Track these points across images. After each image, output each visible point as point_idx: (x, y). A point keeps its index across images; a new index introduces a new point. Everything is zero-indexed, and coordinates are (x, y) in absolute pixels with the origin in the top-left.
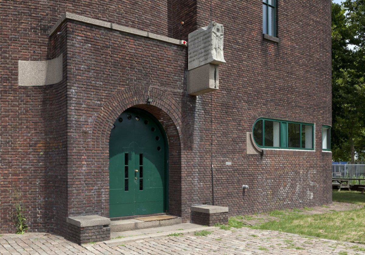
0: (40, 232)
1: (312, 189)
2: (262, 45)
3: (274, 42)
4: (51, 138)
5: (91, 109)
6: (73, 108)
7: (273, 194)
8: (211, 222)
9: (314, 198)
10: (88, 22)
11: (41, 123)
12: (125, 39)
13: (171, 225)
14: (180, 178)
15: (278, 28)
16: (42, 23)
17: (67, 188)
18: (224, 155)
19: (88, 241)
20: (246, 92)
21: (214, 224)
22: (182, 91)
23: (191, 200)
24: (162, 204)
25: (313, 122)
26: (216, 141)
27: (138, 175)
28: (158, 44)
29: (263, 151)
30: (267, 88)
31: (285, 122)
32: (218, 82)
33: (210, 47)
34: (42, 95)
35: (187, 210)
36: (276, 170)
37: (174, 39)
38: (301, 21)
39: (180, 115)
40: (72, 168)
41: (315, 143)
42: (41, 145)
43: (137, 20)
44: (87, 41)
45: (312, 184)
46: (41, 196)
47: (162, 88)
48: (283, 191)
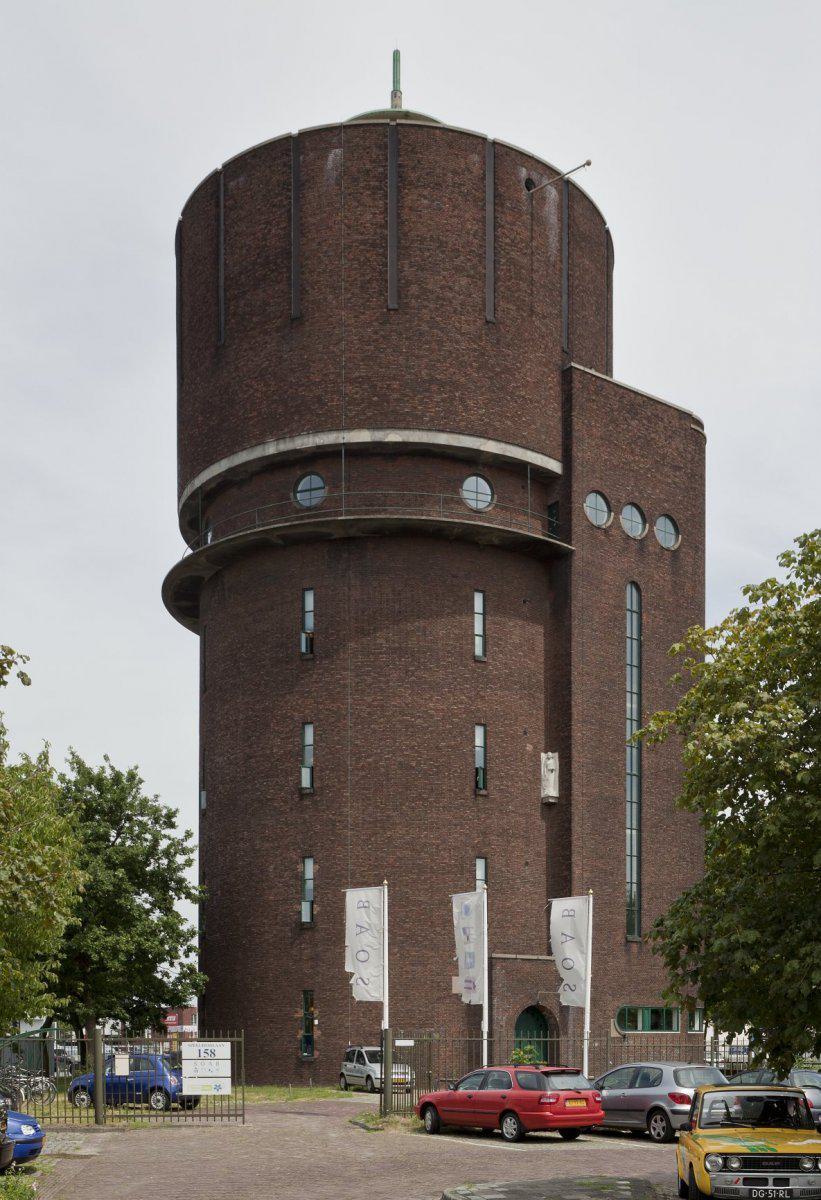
31: (647, 1008)
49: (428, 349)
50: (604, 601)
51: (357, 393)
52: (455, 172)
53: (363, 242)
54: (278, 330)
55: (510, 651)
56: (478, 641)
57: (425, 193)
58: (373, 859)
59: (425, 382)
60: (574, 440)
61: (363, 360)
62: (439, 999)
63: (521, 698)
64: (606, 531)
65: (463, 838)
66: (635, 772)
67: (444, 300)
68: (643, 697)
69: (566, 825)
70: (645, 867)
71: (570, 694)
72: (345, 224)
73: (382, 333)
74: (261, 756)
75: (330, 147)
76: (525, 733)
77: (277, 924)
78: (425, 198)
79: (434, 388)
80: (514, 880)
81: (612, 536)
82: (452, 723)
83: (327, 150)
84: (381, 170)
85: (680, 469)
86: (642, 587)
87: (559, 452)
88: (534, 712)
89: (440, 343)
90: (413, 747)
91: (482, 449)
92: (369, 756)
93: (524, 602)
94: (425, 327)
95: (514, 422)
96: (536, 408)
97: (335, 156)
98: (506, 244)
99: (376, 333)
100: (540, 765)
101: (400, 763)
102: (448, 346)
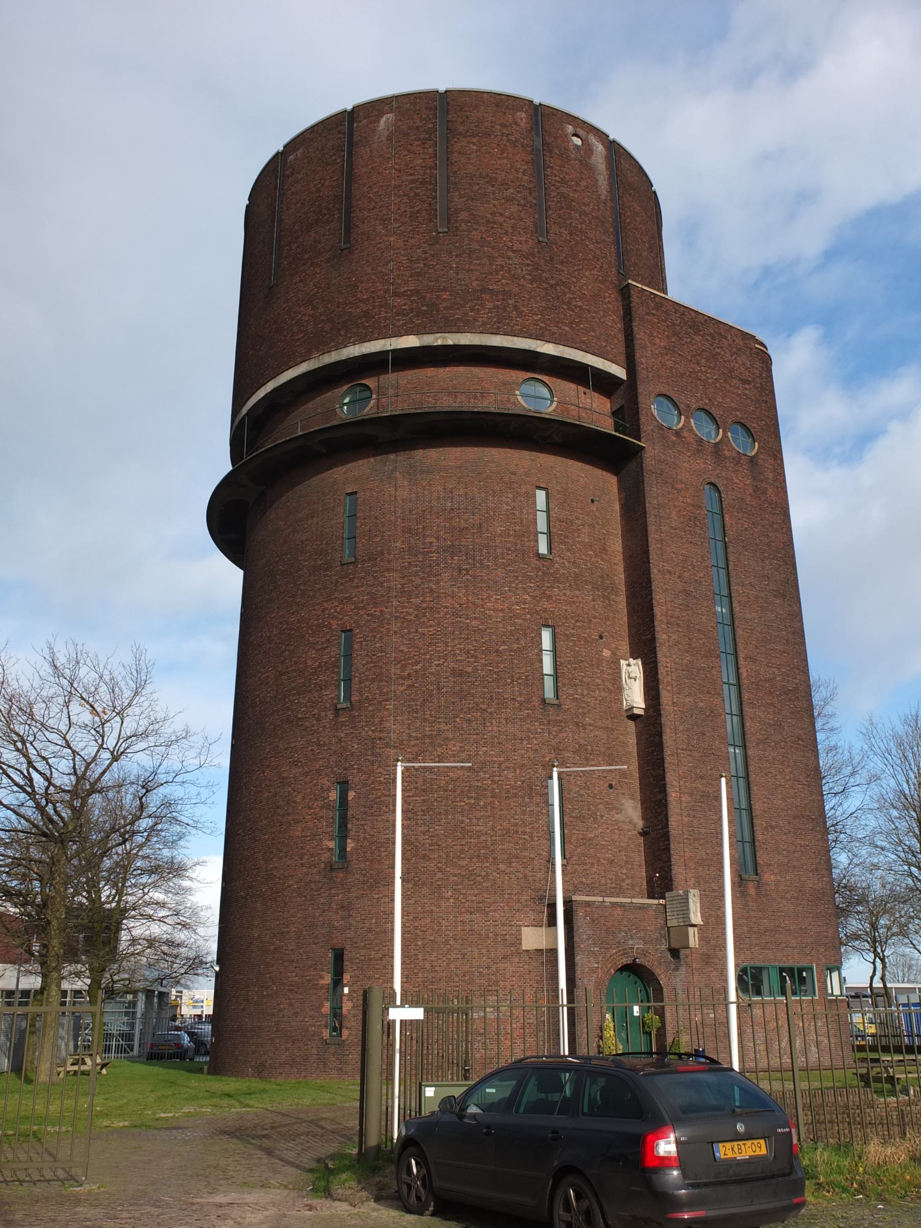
49: (479, 264)
50: (681, 499)
51: (405, 305)
52: (503, 125)
53: (412, 182)
54: (328, 260)
55: (580, 550)
56: (549, 683)
57: (475, 140)
58: (420, 781)
59: (475, 291)
60: (637, 347)
61: (411, 277)
62: (505, 957)
63: (594, 600)
64: (678, 433)
65: (531, 754)
66: (744, 807)
67: (495, 223)
68: (733, 599)
69: (657, 738)
70: (754, 788)
71: (650, 593)
72: (396, 169)
73: (432, 252)
74: (294, 671)
75: (382, 113)
76: (601, 637)
77: (302, 865)
78: (474, 144)
79: (486, 296)
80: (596, 806)
81: (684, 437)
82: (514, 624)
83: (380, 116)
84: (431, 125)
85: (749, 382)
86: (722, 488)
87: (622, 358)
88: (610, 614)
89: (491, 258)
90: (468, 652)
91: (538, 350)
92: (417, 663)
93: (593, 501)
94: (475, 246)
95: (571, 328)
96: (594, 317)
97: (386, 121)
98: (556, 181)
99: (425, 253)
100: (620, 673)
101: (453, 670)
102: (500, 261)
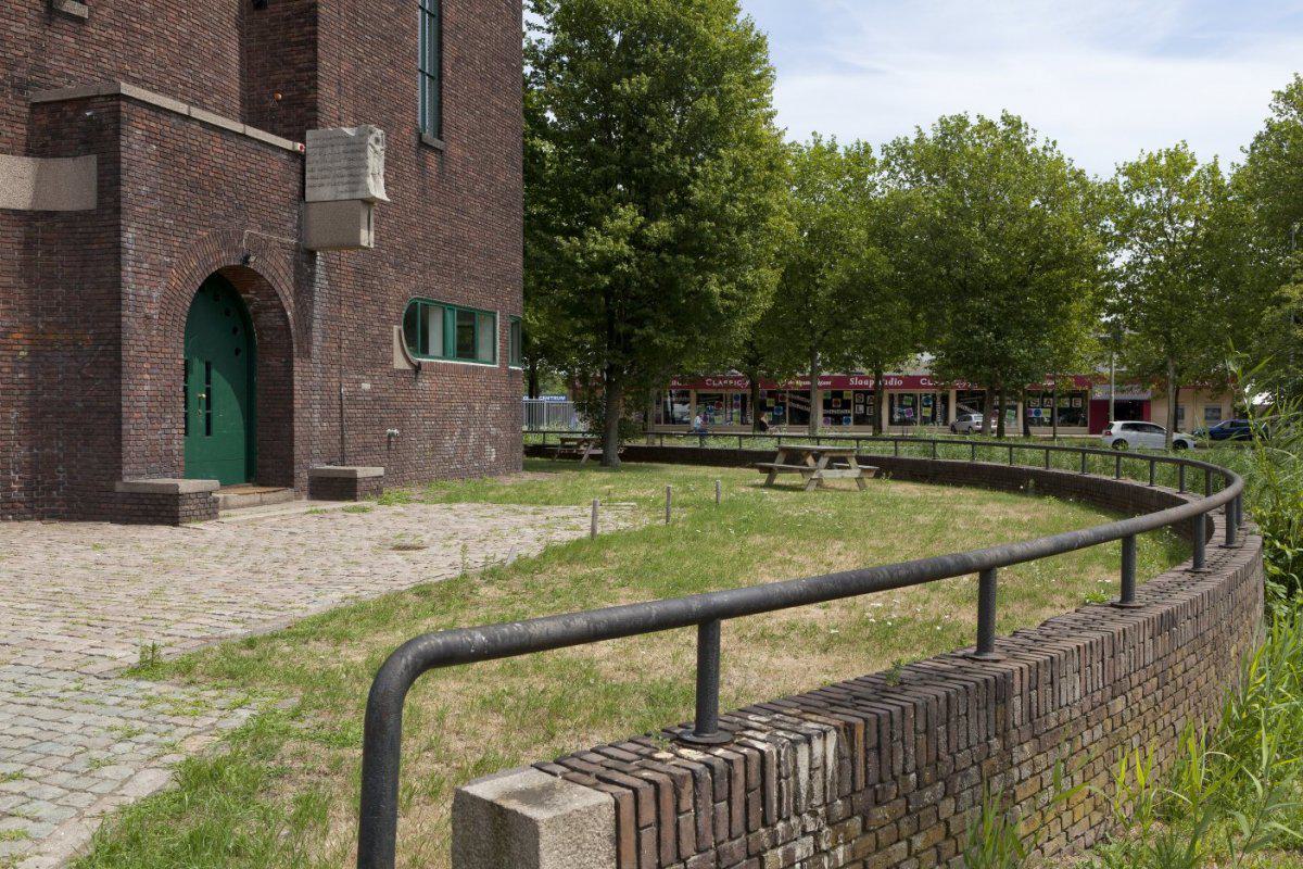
0: (19, 521)
1: (495, 440)
2: (418, 153)
3: (435, 150)
4: (49, 323)
5: (159, 271)
6: (130, 269)
7: (433, 449)
8: (359, 493)
9: (497, 459)
10: (154, 102)
11: (21, 289)
12: (209, 137)
13: (278, 502)
14: (292, 411)
15: (441, 121)
16: (15, 74)
17: (121, 424)
18: (360, 370)
19: (189, 518)
20: (392, 247)
21: (364, 497)
22: (294, 241)
23: (310, 456)
24: (242, 467)
25: (497, 309)
26: (347, 342)
27: (204, 403)
28: (259, 147)
29: (419, 363)
30: (425, 238)
31: (452, 307)
32: (372, 234)
33: (363, 171)
34: (22, 229)
35: (302, 476)
36: (438, 401)
37: (274, 137)
38: (477, 108)
39: (292, 289)
40: (127, 386)
41: (498, 351)
42: (21, 336)
43: (191, 81)
44: (148, 140)
45: (494, 431)
46: (20, 444)
47: (264, 235)
48: (449, 443)
